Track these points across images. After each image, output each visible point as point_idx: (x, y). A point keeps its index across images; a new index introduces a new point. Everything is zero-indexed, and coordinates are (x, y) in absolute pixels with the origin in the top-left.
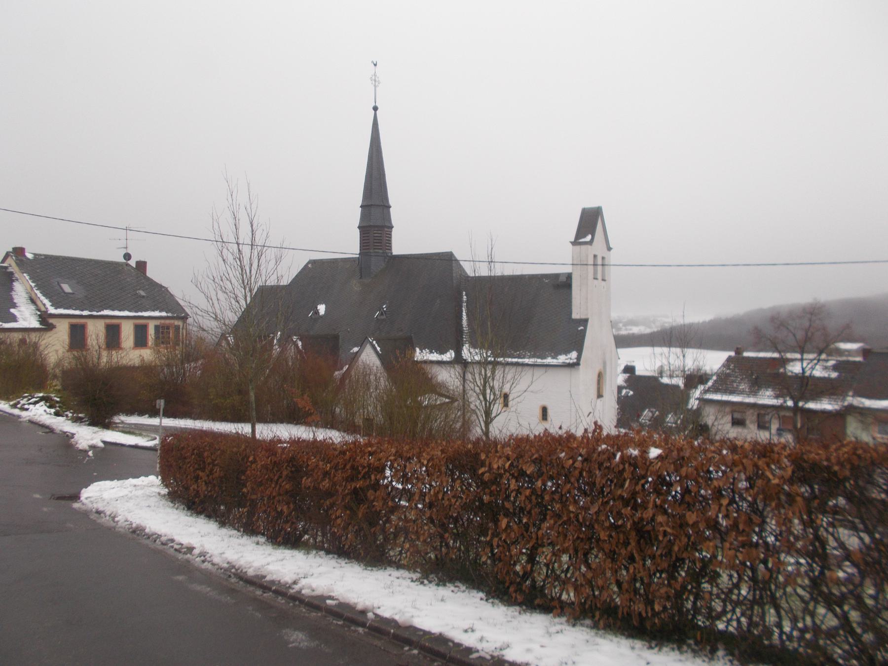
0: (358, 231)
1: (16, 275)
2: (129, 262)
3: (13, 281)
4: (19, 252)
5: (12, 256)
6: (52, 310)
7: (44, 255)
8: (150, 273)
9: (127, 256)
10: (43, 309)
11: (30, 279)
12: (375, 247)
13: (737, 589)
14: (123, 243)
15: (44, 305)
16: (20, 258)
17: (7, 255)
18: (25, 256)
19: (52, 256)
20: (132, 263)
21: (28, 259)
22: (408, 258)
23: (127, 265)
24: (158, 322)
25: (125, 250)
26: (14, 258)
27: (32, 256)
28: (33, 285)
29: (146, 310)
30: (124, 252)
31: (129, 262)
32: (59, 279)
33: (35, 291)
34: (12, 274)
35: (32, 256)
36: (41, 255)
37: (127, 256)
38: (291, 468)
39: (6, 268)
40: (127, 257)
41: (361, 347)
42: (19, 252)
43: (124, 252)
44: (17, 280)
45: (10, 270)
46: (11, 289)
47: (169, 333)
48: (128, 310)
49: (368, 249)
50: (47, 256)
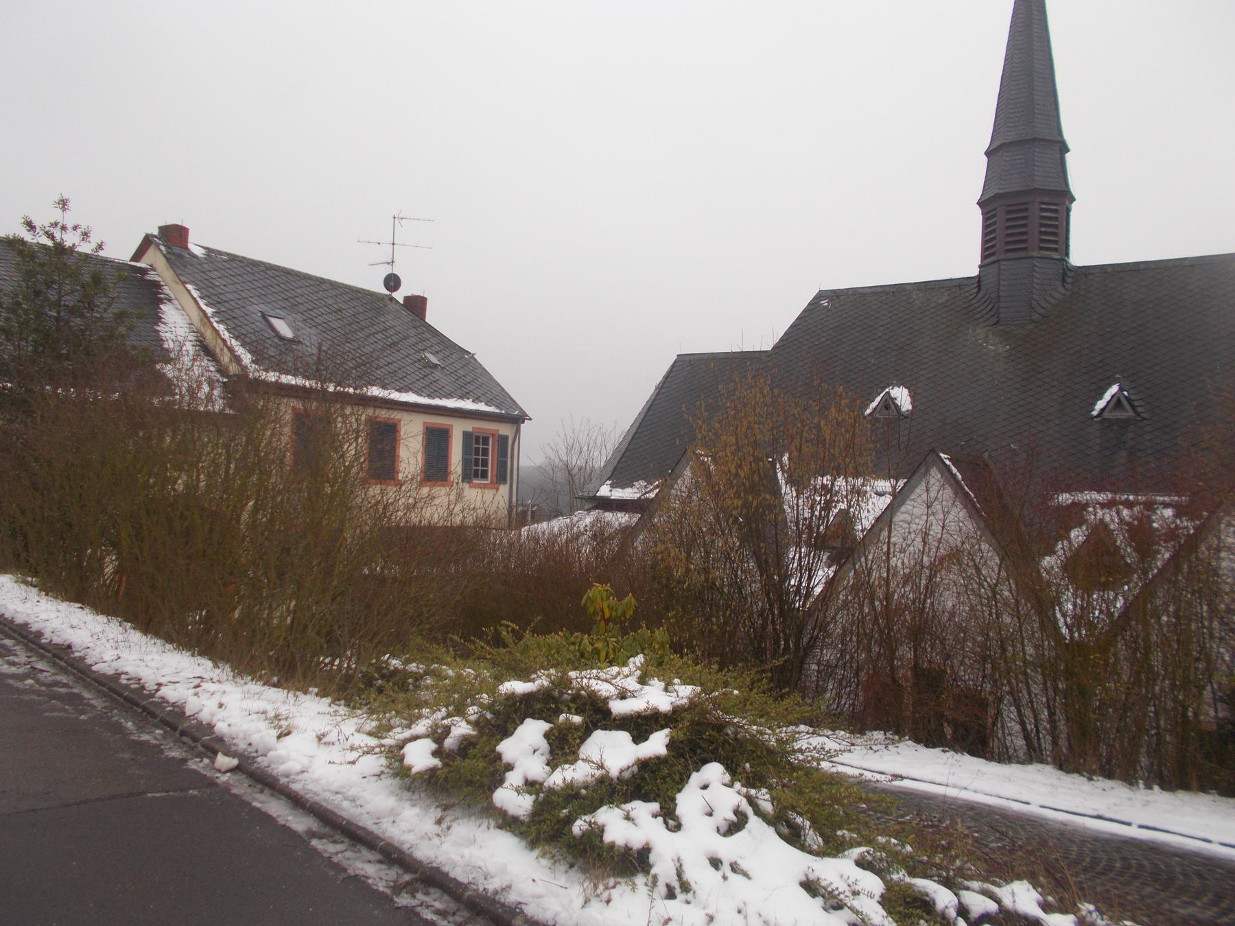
0: (977, 216)
1: (166, 290)
2: (395, 295)
3: (161, 301)
4: (174, 236)
5: (158, 245)
6: (254, 371)
7: (228, 254)
8: (430, 318)
9: (393, 282)
10: (233, 369)
11: (201, 298)
12: (1043, 245)
13: (119, 678)
14: (384, 253)
15: (237, 359)
16: (176, 250)
17: (147, 242)
18: (186, 248)
19: (244, 258)
20: (399, 296)
21: (195, 256)
22: (1138, 271)
23: (392, 299)
24: (469, 426)
25: (389, 267)
26: (162, 248)
27: (203, 251)
28: (209, 311)
29: (448, 396)
30: (387, 270)
31: (395, 295)
32: (263, 308)
33: (215, 325)
34: (157, 285)
35: (203, 251)
36: (220, 253)
37: (393, 282)
38: (800, 761)
39: (144, 271)
40: (392, 284)
41: (909, 479)
42: (174, 236)
43: (386, 271)
44: (170, 300)
45: (152, 276)
46: (158, 319)
47: (485, 452)
48: (415, 392)
49: (1025, 249)
50: (233, 258)
